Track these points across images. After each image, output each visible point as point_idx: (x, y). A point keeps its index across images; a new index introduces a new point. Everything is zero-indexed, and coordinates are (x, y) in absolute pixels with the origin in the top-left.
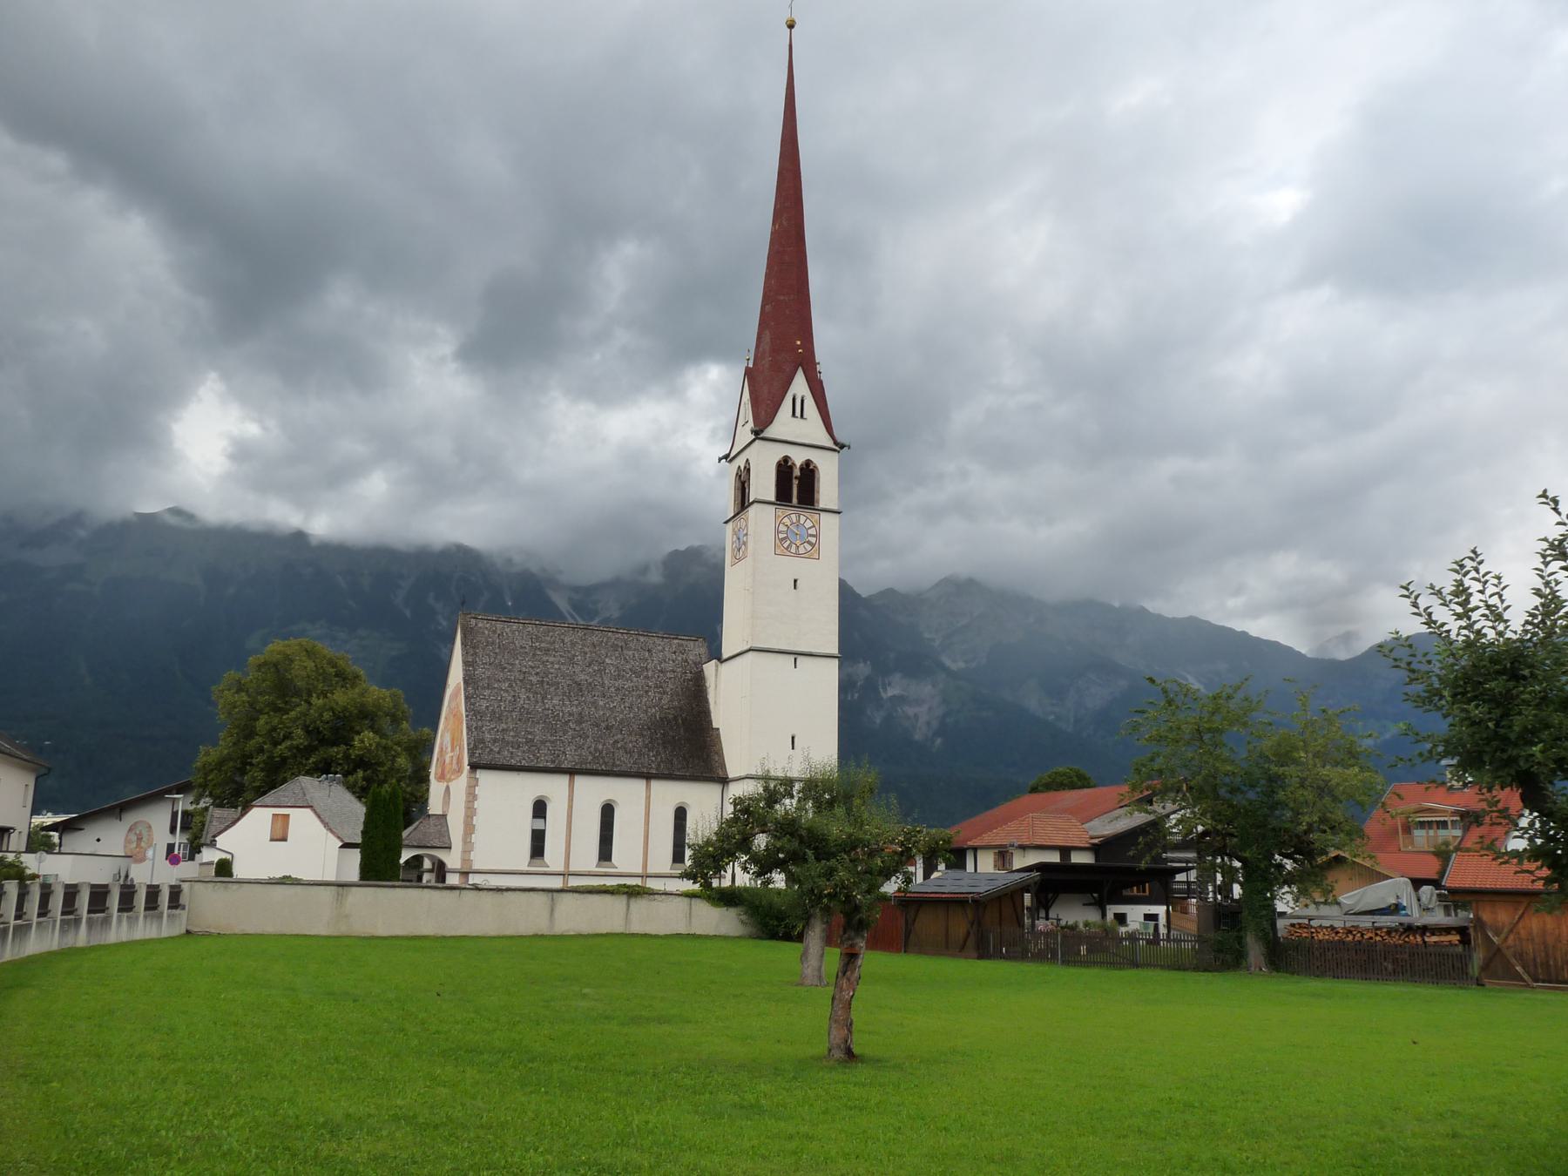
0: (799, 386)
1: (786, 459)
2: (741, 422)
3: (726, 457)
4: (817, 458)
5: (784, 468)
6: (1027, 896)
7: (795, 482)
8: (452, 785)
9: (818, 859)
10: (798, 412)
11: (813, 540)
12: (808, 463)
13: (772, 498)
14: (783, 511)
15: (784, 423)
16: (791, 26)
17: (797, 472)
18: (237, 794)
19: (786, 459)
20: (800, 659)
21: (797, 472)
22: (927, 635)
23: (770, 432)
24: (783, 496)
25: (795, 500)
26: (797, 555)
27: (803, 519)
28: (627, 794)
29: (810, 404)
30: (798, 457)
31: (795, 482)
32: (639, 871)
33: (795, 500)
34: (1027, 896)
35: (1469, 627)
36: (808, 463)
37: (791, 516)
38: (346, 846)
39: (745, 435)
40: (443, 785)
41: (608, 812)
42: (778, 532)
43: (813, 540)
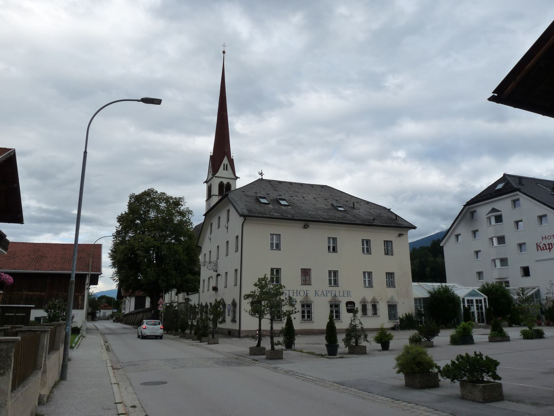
0: (225, 161)
1: (222, 182)
5: (221, 185)
9: (69, 276)
10: (226, 168)
12: (228, 183)
13: (217, 194)
15: (221, 172)
16: (224, 52)
17: (225, 186)
18: (271, 314)
19: (222, 182)
21: (225, 186)
22: (435, 362)
23: (217, 175)
29: (229, 166)
30: (225, 182)
35: (384, 341)
36: (228, 183)
39: (211, 176)
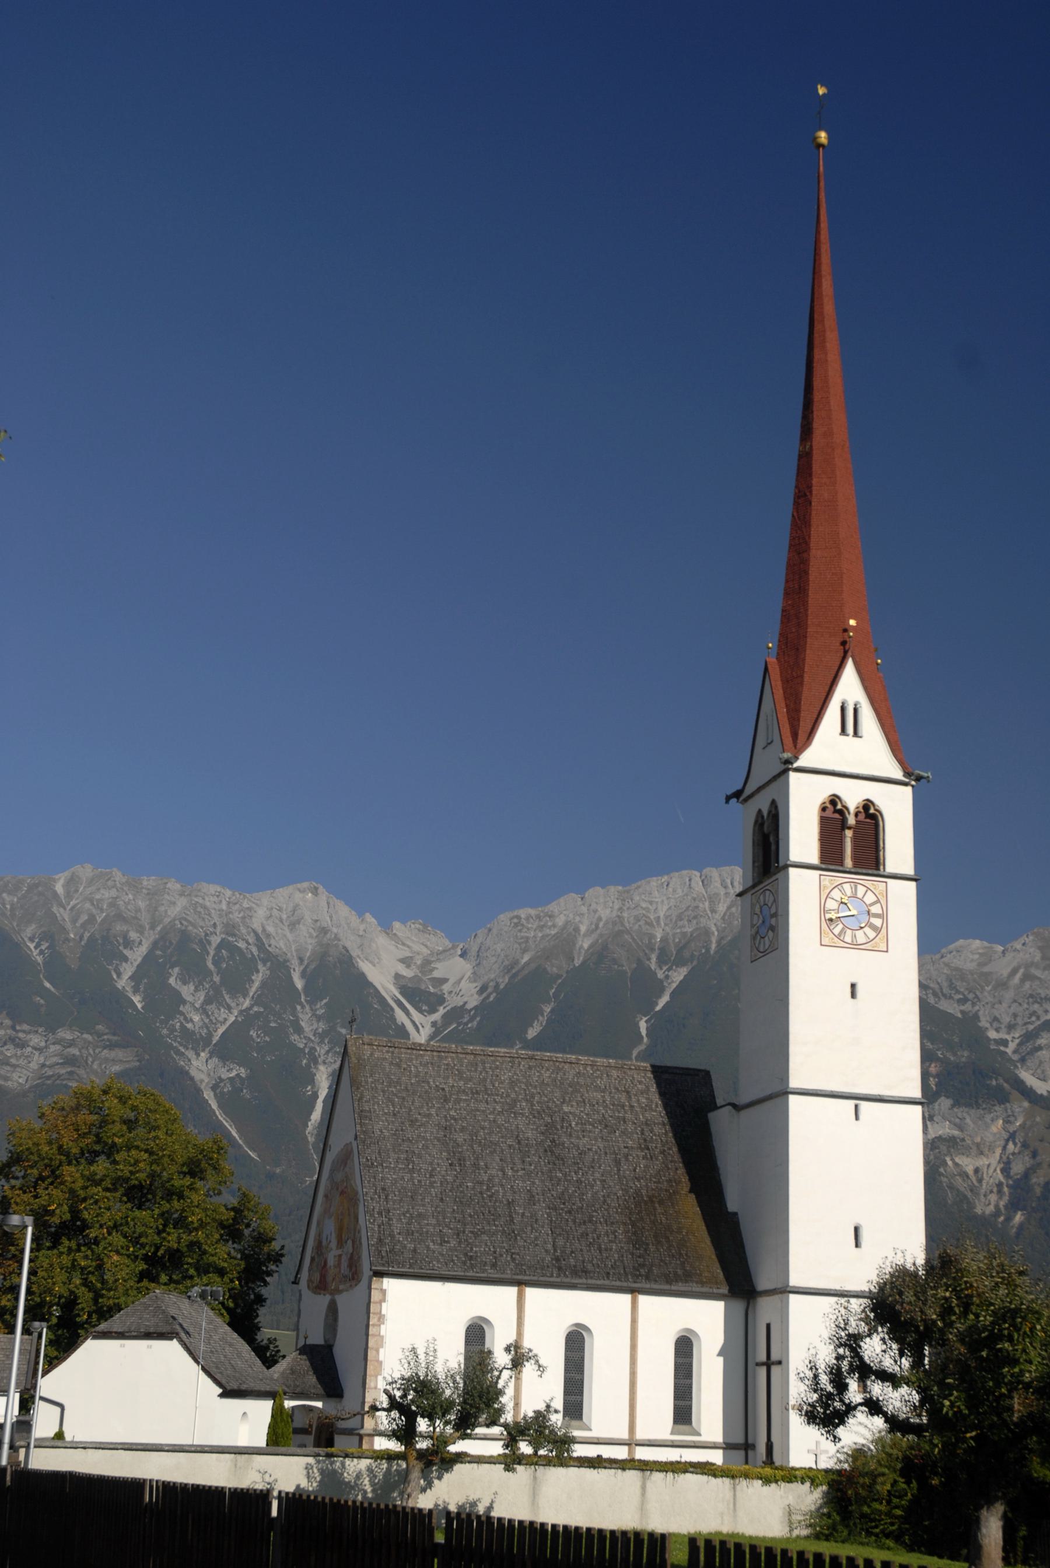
1: (834, 800)
2: (761, 741)
3: (737, 794)
4: (877, 793)
6: (531, 1033)
7: (849, 833)
8: (341, 1300)
11: (877, 922)
14: (832, 878)
19: (834, 800)
20: (864, 1105)
24: (830, 857)
25: (849, 863)
26: (855, 945)
27: (861, 890)
28: (602, 1311)
30: (853, 795)
31: (849, 833)
32: (624, 1435)
33: (849, 863)
34: (531, 1033)
37: (845, 886)
38: (780, 1363)
40: (324, 1300)
41: (576, 1343)
42: (823, 910)
43: (877, 922)
